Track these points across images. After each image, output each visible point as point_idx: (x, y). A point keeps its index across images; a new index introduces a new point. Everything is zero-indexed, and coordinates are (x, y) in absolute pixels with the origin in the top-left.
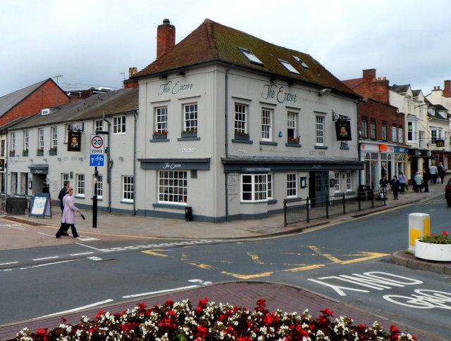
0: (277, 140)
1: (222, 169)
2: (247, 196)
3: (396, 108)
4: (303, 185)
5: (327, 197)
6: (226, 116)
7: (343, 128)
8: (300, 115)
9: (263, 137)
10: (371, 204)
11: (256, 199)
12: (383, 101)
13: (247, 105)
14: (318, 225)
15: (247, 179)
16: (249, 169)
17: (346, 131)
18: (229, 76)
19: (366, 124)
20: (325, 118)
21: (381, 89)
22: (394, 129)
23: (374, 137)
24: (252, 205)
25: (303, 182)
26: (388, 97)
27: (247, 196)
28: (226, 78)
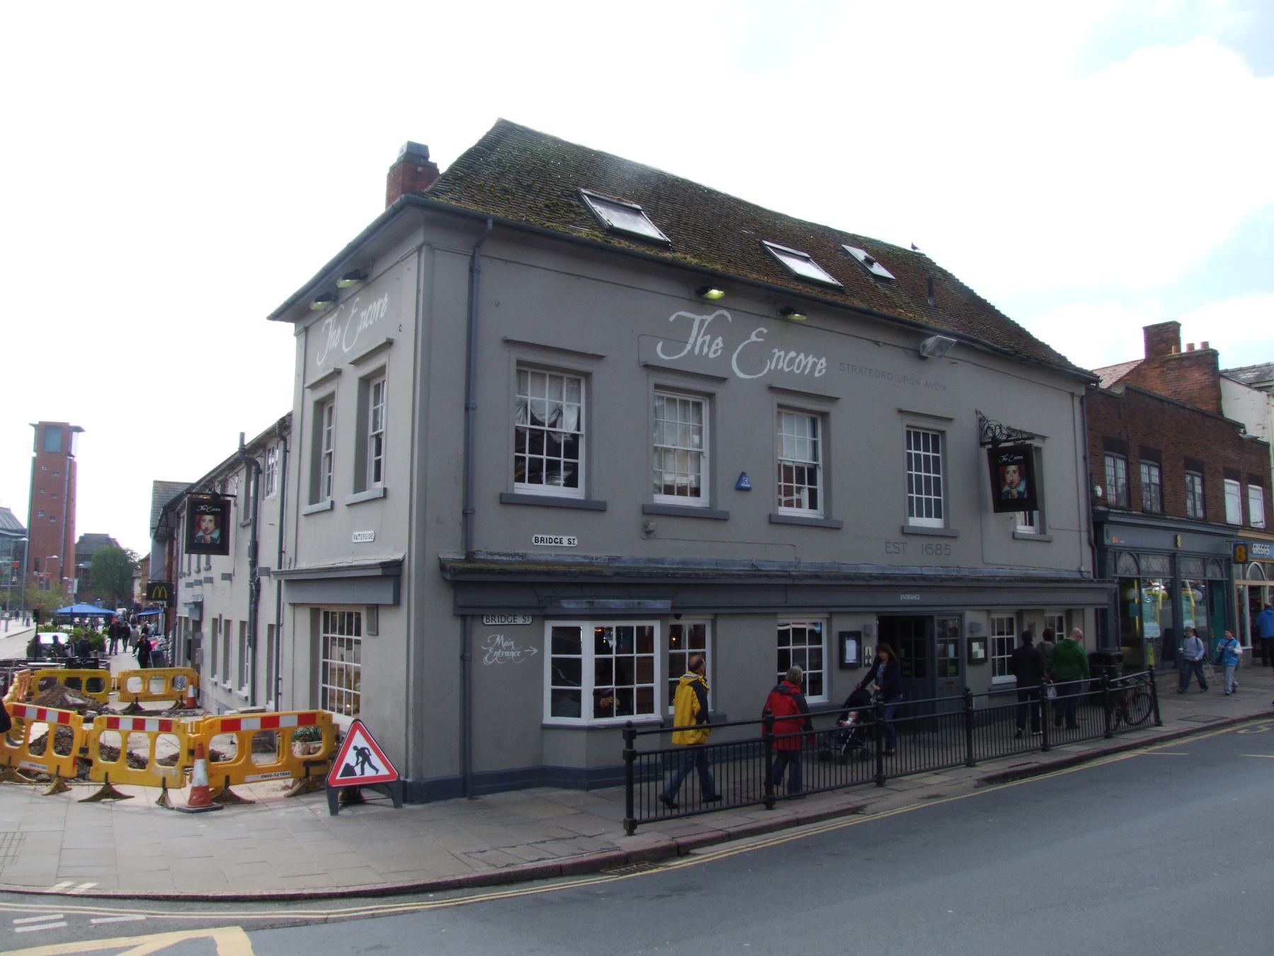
0: (729, 501)
1: (443, 602)
2: (566, 702)
3: (1237, 427)
4: (851, 656)
5: (967, 698)
6: (468, 408)
7: (1012, 468)
8: (835, 419)
9: (520, 479)
10: (1102, 723)
11: (600, 711)
12: (1208, 408)
13: (943, 433)
14: (729, 837)
15: (567, 641)
16: (569, 605)
17: (1021, 477)
18: (484, 264)
19: (1121, 464)
20: (949, 436)
21: (1197, 377)
22: (1231, 489)
23: (1156, 508)
24: (584, 735)
25: (851, 646)
26: (1218, 398)
27: (566, 702)
28: (473, 271)
